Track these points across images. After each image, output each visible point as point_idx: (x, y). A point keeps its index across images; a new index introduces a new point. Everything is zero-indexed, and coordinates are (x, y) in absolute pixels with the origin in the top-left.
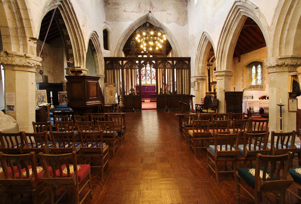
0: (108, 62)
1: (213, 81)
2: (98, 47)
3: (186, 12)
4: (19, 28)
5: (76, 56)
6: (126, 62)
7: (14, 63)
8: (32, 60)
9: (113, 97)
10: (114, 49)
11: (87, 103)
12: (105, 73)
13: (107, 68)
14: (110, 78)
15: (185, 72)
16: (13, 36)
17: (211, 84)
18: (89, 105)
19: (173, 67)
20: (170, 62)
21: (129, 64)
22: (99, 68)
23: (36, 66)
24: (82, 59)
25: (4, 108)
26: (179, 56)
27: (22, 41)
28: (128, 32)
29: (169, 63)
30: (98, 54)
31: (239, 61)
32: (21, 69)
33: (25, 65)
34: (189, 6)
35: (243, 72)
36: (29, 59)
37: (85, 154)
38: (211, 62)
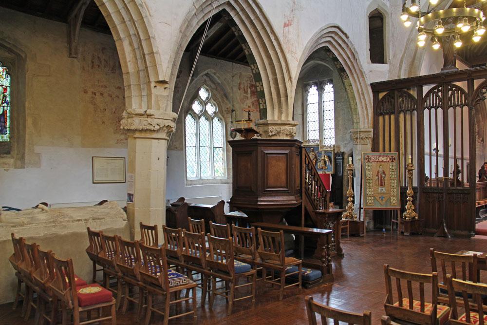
0: (381, 95)
1: (413, 186)
2: (350, 61)
4: (141, 70)
5: (271, 94)
7: (133, 128)
8: (155, 118)
9: (384, 190)
10: (399, 56)
11: (260, 199)
13: (379, 111)
14: (387, 139)
16: (135, 85)
18: (262, 205)
21: (440, 94)
22: (357, 114)
23: (165, 128)
24: (283, 99)
27: (146, 90)
29: (459, 88)
30: (353, 77)
32: (143, 135)
33: (145, 128)
36: (152, 118)
37: (150, 285)
38: (47, 206)
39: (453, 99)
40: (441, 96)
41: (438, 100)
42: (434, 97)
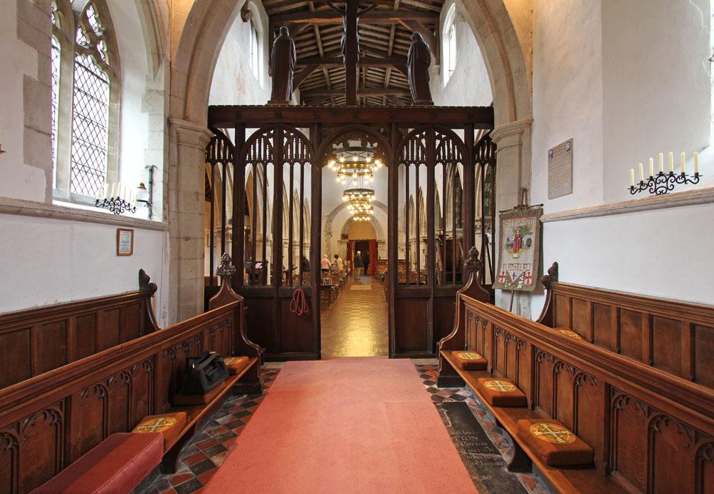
21: (423, 141)
29: (299, 135)
39: (289, 150)
40: (425, 146)
41: (456, 150)
42: (415, 145)
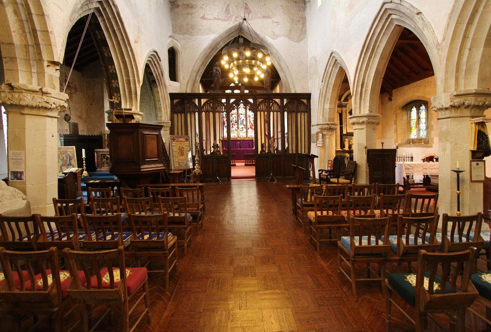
0: (175, 101)
1: (348, 132)
2: (160, 76)
3: (303, 20)
4: (31, 46)
5: (125, 91)
6: (205, 100)
7: (23, 103)
8: (51, 97)
9: (184, 158)
10: (187, 79)
11: (141, 167)
12: (172, 119)
13: (174, 110)
14: (180, 128)
15: (302, 118)
16: (22, 59)
17: (344, 137)
18: (146, 171)
19: (282, 109)
20: (278, 100)
21: (211, 104)
22: (161, 111)
23: (59, 108)
24: (133, 96)
25: (7, 177)
26: (293, 92)
27: (36, 67)
28: (208, 52)
29: (276, 102)
30: (160, 88)
31: (390, 99)
32: (35, 112)
33: (40, 106)
34: (308, 9)
35: (396, 117)
36: (48, 96)
38: (344, 101)
